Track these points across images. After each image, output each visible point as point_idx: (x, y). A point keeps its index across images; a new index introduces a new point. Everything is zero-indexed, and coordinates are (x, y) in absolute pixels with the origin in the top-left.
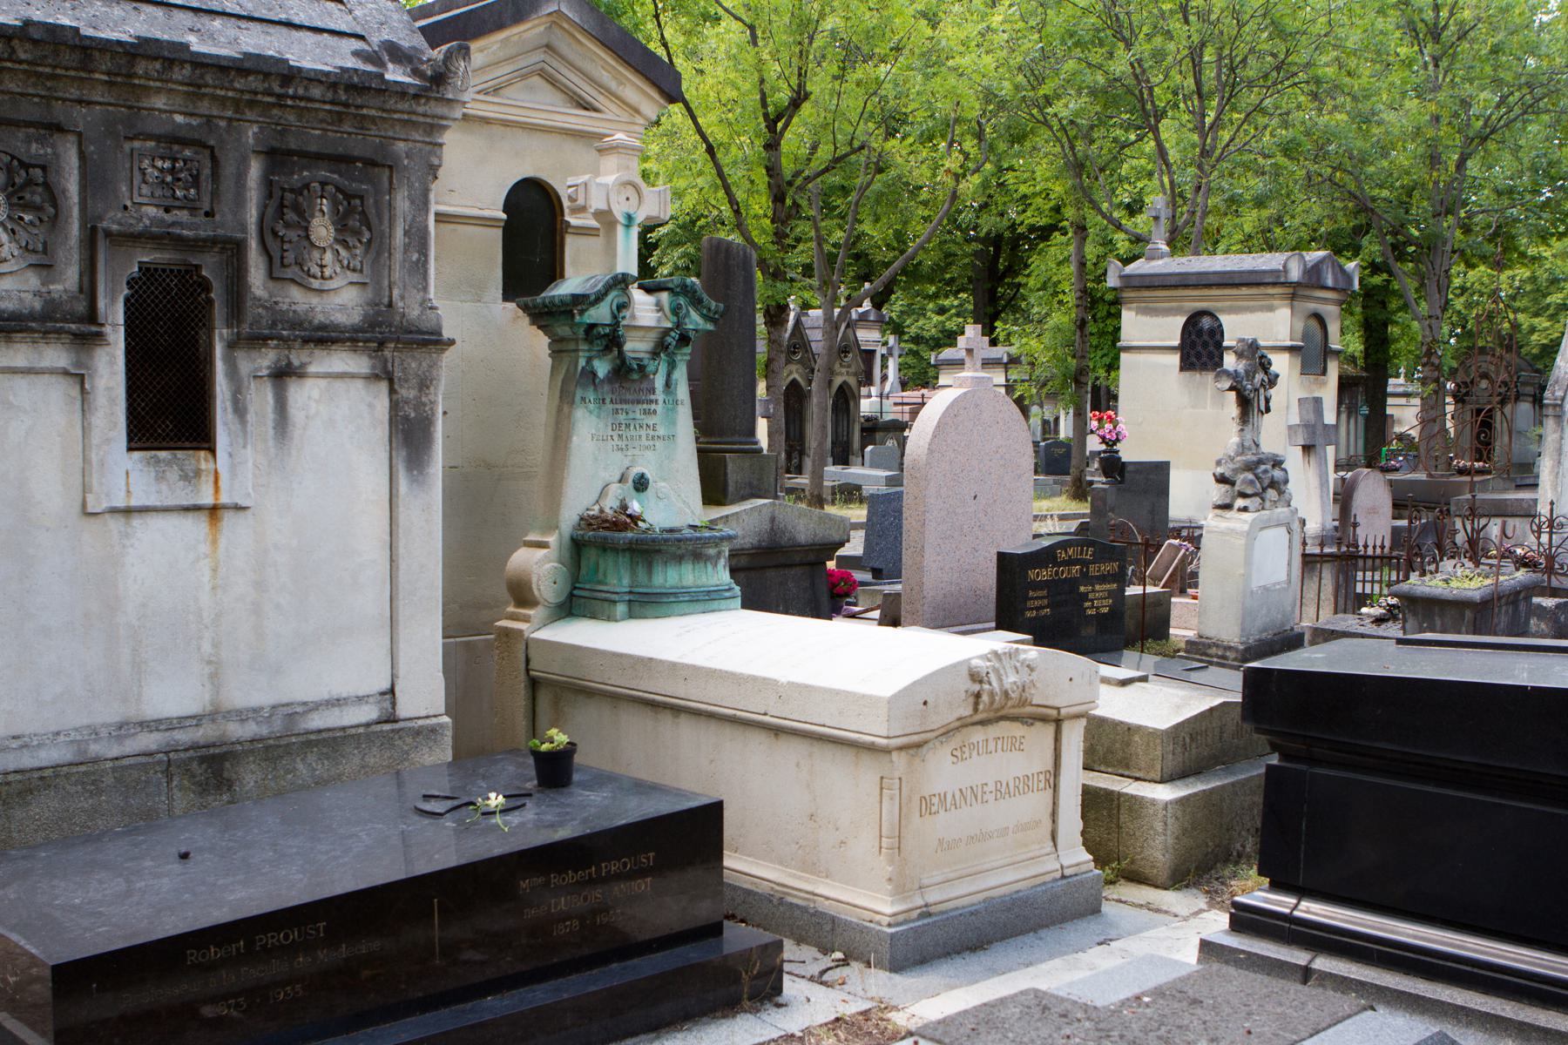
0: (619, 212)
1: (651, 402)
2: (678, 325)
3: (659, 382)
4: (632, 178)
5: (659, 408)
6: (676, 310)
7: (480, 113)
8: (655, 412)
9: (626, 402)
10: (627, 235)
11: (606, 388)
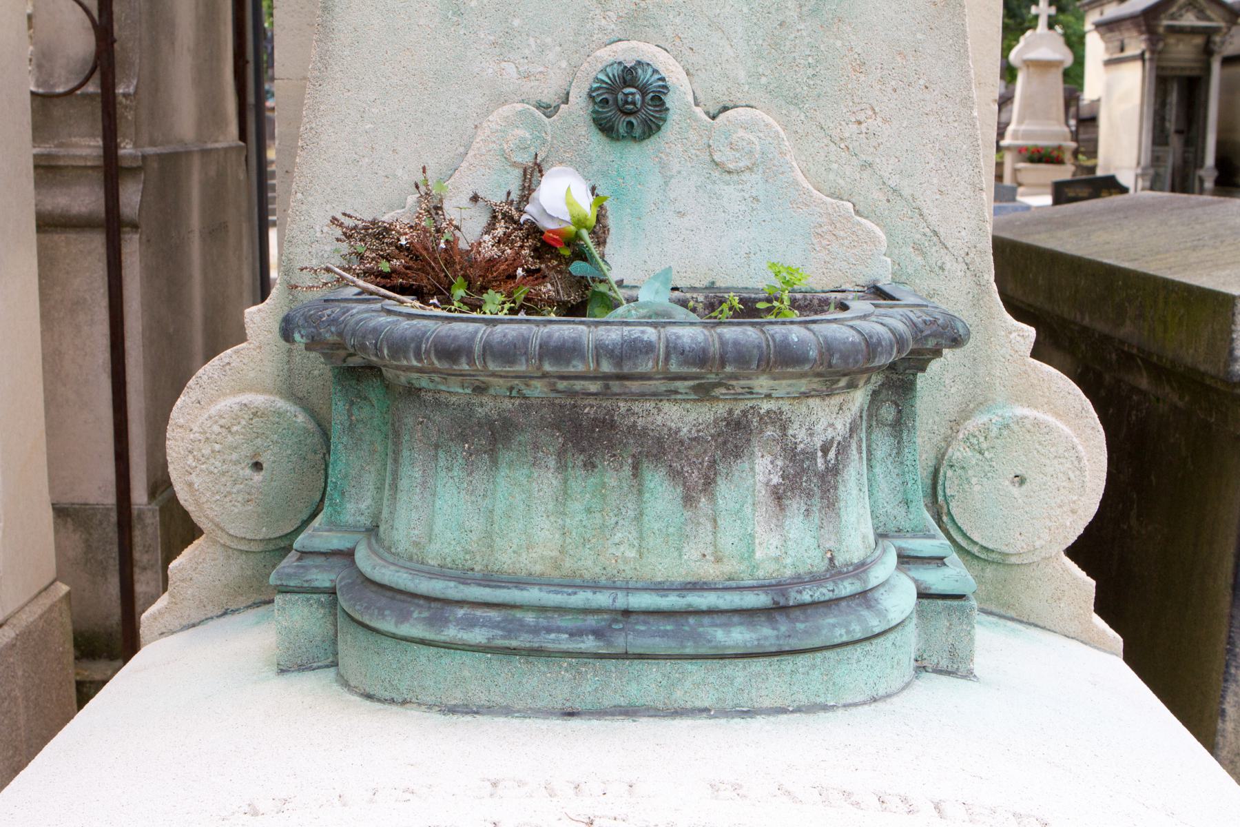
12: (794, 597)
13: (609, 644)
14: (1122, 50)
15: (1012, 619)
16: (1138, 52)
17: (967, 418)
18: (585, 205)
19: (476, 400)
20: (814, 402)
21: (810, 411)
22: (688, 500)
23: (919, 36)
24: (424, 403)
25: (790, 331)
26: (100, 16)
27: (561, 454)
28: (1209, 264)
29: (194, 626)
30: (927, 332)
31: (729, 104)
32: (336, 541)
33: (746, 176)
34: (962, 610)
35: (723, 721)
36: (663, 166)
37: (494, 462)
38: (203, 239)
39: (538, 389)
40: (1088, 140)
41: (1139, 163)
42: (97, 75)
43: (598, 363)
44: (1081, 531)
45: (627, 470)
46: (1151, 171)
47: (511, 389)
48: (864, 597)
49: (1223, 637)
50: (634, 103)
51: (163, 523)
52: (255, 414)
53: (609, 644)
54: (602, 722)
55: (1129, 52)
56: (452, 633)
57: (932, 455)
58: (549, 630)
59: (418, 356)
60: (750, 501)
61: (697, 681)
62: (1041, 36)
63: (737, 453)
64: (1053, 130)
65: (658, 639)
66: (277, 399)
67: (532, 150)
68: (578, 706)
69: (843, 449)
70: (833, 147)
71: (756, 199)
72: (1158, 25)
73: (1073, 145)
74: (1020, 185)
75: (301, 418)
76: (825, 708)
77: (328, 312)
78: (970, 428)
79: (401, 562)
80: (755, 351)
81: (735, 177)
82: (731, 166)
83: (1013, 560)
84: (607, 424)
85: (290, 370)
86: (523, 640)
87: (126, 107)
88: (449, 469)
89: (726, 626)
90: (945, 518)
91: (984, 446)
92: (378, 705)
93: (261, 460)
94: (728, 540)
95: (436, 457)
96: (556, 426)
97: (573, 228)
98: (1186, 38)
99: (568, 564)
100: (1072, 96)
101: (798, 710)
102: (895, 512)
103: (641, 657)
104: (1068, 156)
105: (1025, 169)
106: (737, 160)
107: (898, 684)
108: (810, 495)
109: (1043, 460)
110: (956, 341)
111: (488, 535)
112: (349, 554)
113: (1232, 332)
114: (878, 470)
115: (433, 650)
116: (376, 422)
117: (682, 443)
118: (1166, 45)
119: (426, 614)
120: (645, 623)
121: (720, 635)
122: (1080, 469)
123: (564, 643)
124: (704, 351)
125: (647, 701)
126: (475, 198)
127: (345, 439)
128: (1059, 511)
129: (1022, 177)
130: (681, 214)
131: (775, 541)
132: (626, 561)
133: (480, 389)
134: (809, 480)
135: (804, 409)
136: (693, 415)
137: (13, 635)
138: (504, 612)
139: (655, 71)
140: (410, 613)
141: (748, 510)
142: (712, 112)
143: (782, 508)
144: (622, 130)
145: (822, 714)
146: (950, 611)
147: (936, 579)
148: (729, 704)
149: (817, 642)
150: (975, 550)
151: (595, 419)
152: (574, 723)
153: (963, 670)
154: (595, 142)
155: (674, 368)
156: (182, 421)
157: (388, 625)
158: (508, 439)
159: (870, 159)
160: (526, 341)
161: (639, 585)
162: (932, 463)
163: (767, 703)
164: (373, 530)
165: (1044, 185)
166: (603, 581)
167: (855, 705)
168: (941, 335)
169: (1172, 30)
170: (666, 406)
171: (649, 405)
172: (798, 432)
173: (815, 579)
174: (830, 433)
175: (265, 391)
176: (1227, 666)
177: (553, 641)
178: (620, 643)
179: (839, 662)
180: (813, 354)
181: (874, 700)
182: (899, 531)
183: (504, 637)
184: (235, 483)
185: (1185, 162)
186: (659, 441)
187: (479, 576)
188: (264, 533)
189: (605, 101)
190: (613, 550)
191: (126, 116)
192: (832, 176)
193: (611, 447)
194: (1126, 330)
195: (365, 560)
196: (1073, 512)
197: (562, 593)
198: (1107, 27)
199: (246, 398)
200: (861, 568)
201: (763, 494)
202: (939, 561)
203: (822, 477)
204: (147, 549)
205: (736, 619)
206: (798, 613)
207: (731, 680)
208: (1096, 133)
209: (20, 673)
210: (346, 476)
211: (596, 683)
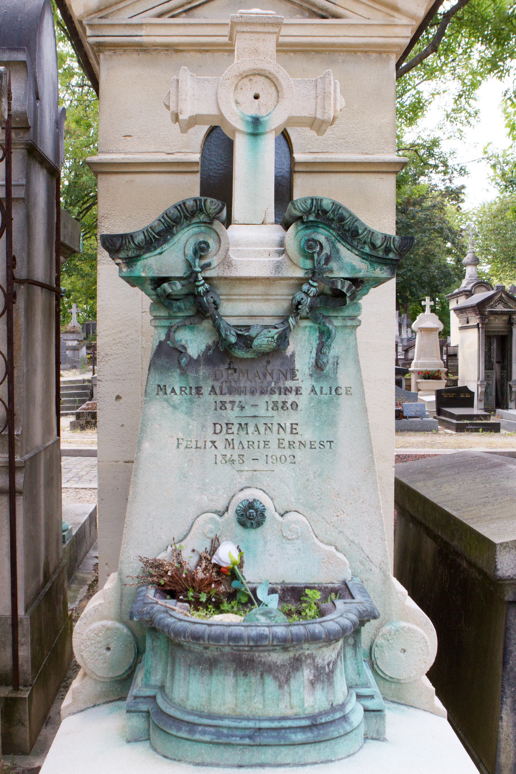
0: (236, 119)
1: (287, 391)
2: (314, 273)
3: (303, 363)
4: (260, 66)
5: (303, 400)
6: (309, 249)
7: (159, 40)
8: (295, 406)
9: (240, 391)
10: (255, 149)
11: (203, 371)
12: (319, 721)
13: (254, 741)
14: (468, 322)
15: (403, 704)
16: (476, 324)
17: (382, 627)
18: (236, 557)
19: (204, 651)
20: (324, 649)
22: (281, 687)
23: (360, 484)
24: (185, 650)
25: (315, 628)
26: (9, 405)
27: (235, 671)
28: (489, 518)
29: (82, 711)
30: (364, 615)
31: (288, 510)
32: (149, 692)
33: (295, 541)
34: (380, 715)
35: (295, 768)
36: (264, 538)
37: (211, 673)
38: (45, 488)
39: (227, 649)
40: (453, 366)
41: (479, 379)
42: (7, 428)
43: (249, 642)
44: (428, 669)
45: (259, 676)
46: (485, 383)
47: (217, 649)
48: (345, 718)
49: (500, 685)
50: (253, 516)
51: (31, 623)
52: (108, 629)
53: (254, 741)
55: (470, 324)
56: (197, 737)
57: (369, 641)
58: (233, 736)
59: (184, 637)
61: (286, 754)
62: (427, 316)
63: (297, 669)
64: (435, 362)
65: (271, 739)
66: (116, 622)
67: (215, 533)
68: (243, 763)
69: (335, 663)
70: (328, 526)
71: (299, 549)
72: (484, 311)
73: (446, 370)
74: (419, 390)
75: (126, 631)
76: (331, 761)
77: (145, 609)
78: (384, 631)
80: (303, 637)
81: (291, 542)
82: (290, 538)
83: (402, 681)
84: (251, 661)
85: (121, 611)
86: (223, 740)
87: (17, 440)
88: (195, 675)
89: (295, 733)
90: (375, 666)
91: (389, 638)
92: (169, 761)
93: (110, 646)
94: (295, 701)
95: (189, 670)
96: (234, 661)
97: (232, 566)
98: (500, 317)
99: (238, 711)
100: (444, 344)
101: (322, 762)
103: (266, 745)
104: (443, 375)
105: (422, 382)
106: (292, 535)
107: (357, 749)
108: (323, 682)
109: (412, 643)
110: (375, 618)
111: (209, 699)
112: (154, 698)
113: (495, 558)
114: (348, 662)
115: (190, 743)
116: (162, 646)
117: (278, 666)
118: (489, 320)
119: (187, 729)
120: (267, 733)
122: (427, 646)
123: (238, 741)
124: (286, 638)
126: (193, 551)
127: (151, 653)
129: (420, 387)
130: (271, 555)
132: (259, 709)
133: (206, 648)
134: (323, 677)
138: (216, 729)
139: (261, 503)
140: (182, 728)
141: (302, 689)
142: (282, 513)
144: (249, 525)
145: (330, 764)
146: (376, 716)
147: (371, 704)
148: (297, 761)
149: (327, 738)
150: (387, 678)
151: (247, 659)
154: (239, 529)
155: (275, 643)
156: (79, 631)
157: (174, 732)
158: (216, 666)
159: (342, 530)
160: (223, 635)
162: (369, 644)
163: (310, 761)
164: (162, 688)
165: (431, 390)
166: (251, 717)
167: (342, 759)
168: (370, 616)
169: (492, 313)
170: (272, 654)
171: (266, 654)
172: (319, 661)
173: (326, 713)
174: (330, 659)
175: (111, 619)
178: (258, 741)
179: (336, 744)
180: (323, 636)
181: (349, 756)
182: (357, 685)
183: (216, 739)
184: (100, 655)
185: (502, 377)
186: (270, 666)
187: (206, 714)
188: (111, 675)
189: (243, 515)
190: (254, 705)
191: (18, 444)
192: (328, 536)
193: (253, 668)
194: (455, 543)
195: (160, 700)
196: (425, 662)
198: (460, 311)
199: (105, 622)
200: (343, 706)
201: (307, 683)
202: (372, 697)
203: (328, 675)
204: (24, 636)
205: (299, 730)
206: (320, 726)
207: (298, 753)
208: (457, 362)
210: (151, 667)
211: (248, 756)
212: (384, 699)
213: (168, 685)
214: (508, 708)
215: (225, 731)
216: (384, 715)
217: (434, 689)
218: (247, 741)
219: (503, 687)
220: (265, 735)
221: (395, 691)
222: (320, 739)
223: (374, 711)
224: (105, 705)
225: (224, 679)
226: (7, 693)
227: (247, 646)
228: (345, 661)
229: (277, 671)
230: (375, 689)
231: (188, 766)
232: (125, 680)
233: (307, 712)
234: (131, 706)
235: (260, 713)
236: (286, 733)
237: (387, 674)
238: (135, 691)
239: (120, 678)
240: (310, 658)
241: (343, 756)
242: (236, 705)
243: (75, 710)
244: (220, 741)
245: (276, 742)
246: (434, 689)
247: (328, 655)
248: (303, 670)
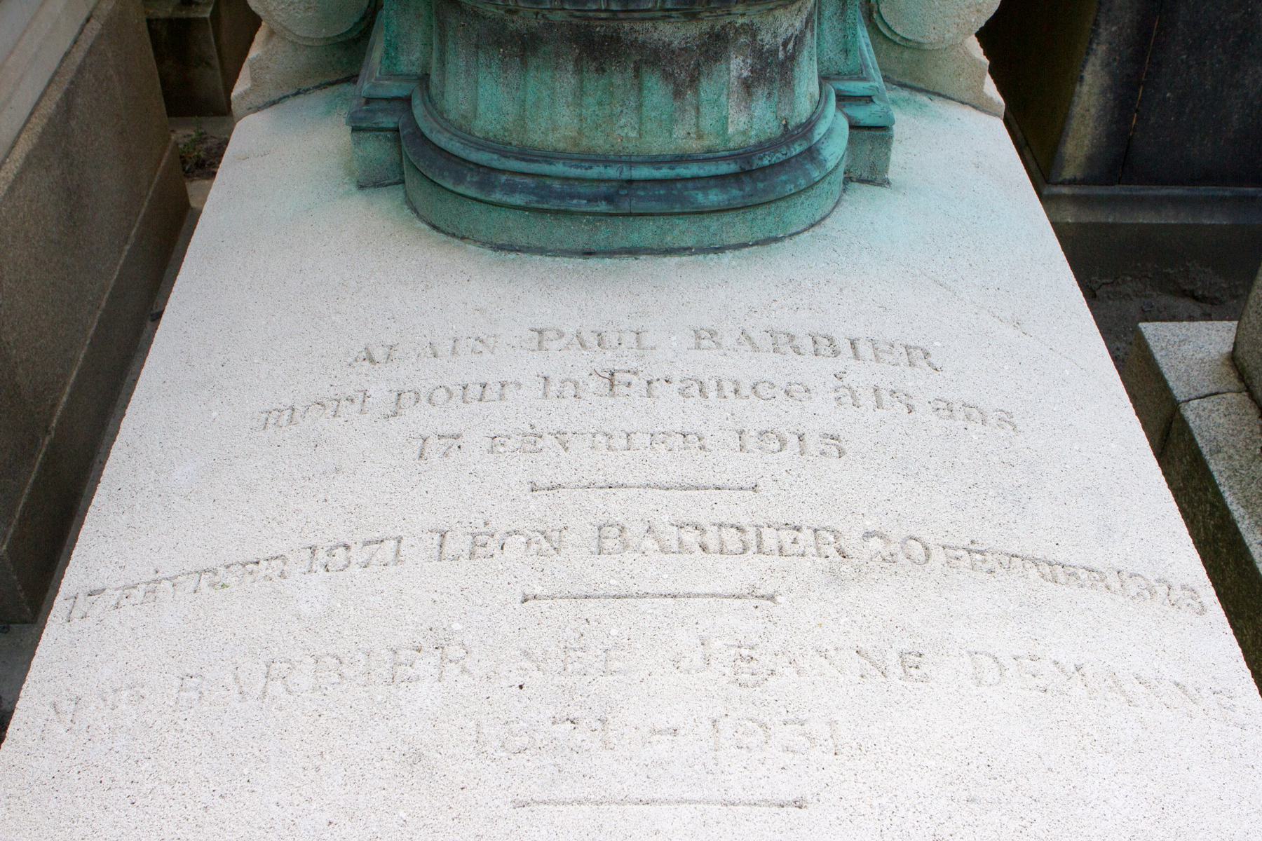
12: (757, 164)
19: (508, 17)
21: (776, 19)
22: (678, 94)
27: (577, 61)
29: (274, 103)
34: (882, 138)
35: (701, 257)
37: (524, 64)
45: (630, 73)
47: (537, 14)
48: (812, 154)
54: (612, 260)
56: (497, 196)
58: (572, 197)
60: (725, 92)
61: (683, 231)
68: (594, 248)
69: (799, 40)
76: (776, 240)
79: (453, 130)
83: (926, 47)
84: (614, 39)
86: (553, 204)
89: (704, 189)
90: (875, 15)
94: (708, 123)
99: (584, 142)
101: (756, 243)
102: (836, 58)
112: (407, 100)
114: (826, 26)
115: (484, 207)
117: (673, 52)
120: (644, 189)
121: (700, 197)
125: (647, 244)
128: (966, 11)
131: (744, 118)
135: (771, 19)
136: (683, 31)
137: (99, 26)
141: (723, 99)
143: (750, 94)
145: (774, 245)
147: (864, 114)
149: (772, 197)
150: (897, 39)
151: (605, 36)
152: (592, 262)
153: (879, 180)
161: (639, 159)
163: (733, 241)
164: (424, 79)
167: (798, 233)
171: (648, 25)
172: (766, 38)
176: (1091, 43)
177: (576, 205)
178: (625, 206)
181: (812, 226)
182: (839, 74)
183: (537, 202)
186: (655, 51)
187: (516, 150)
188: (323, 33)
190: (619, 132)
195: (418, 110)
196: (978, 11)
197: (581, 167)
200: (808, 126)
201: (735, 83)
202: (868, 99)
205: (712, 182)
207: (708, 228)
209: (110, 55)
211: (603, 235)
212: (886, 79)
213: (434, 78)
214: (1098, 62)
215: (557, 185)
216: (891, 137)
217: (987, 62)
218: (603, 207)
219: (1096, 23)
220: (641, 193)
221: (913, 71)
222: (756, 200)
223: (869, 128)
224: (318, 92)
225: (552, 77)
226: (170, 10)
227: (606, 11)
228: (820, 24)
229: (670, 62)
230: (876, 84)
231: (481, 250)
232: (356, 41)
233: (731, 145)
234: (361, 119)
235: (631, 148)
236: (687, 189)
237: (898, 31)
238: (366, 86)
239: (343, 39)
240: (746, 33)
241: (802, 227)
242: (580, 132)
243: (260, 101)
244: (546, 206)
245: (664, 207)
246: (986, 62)
247: (785, 25)
248: (728, 59)
